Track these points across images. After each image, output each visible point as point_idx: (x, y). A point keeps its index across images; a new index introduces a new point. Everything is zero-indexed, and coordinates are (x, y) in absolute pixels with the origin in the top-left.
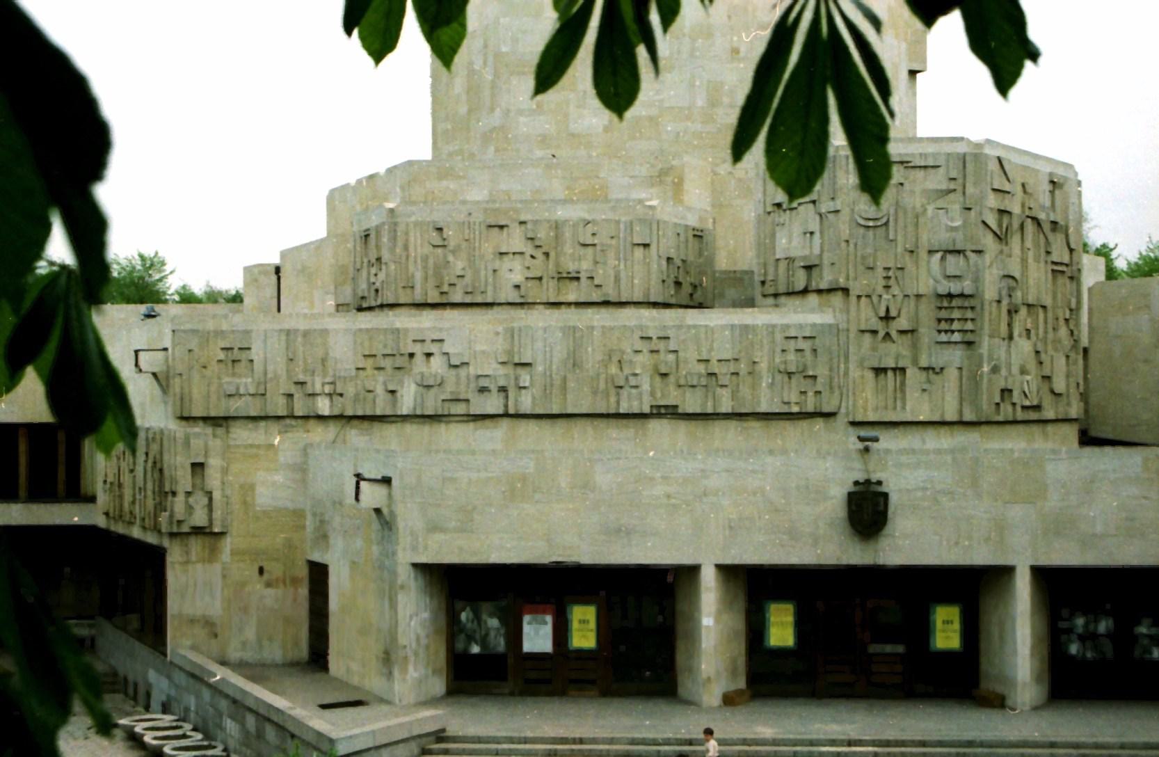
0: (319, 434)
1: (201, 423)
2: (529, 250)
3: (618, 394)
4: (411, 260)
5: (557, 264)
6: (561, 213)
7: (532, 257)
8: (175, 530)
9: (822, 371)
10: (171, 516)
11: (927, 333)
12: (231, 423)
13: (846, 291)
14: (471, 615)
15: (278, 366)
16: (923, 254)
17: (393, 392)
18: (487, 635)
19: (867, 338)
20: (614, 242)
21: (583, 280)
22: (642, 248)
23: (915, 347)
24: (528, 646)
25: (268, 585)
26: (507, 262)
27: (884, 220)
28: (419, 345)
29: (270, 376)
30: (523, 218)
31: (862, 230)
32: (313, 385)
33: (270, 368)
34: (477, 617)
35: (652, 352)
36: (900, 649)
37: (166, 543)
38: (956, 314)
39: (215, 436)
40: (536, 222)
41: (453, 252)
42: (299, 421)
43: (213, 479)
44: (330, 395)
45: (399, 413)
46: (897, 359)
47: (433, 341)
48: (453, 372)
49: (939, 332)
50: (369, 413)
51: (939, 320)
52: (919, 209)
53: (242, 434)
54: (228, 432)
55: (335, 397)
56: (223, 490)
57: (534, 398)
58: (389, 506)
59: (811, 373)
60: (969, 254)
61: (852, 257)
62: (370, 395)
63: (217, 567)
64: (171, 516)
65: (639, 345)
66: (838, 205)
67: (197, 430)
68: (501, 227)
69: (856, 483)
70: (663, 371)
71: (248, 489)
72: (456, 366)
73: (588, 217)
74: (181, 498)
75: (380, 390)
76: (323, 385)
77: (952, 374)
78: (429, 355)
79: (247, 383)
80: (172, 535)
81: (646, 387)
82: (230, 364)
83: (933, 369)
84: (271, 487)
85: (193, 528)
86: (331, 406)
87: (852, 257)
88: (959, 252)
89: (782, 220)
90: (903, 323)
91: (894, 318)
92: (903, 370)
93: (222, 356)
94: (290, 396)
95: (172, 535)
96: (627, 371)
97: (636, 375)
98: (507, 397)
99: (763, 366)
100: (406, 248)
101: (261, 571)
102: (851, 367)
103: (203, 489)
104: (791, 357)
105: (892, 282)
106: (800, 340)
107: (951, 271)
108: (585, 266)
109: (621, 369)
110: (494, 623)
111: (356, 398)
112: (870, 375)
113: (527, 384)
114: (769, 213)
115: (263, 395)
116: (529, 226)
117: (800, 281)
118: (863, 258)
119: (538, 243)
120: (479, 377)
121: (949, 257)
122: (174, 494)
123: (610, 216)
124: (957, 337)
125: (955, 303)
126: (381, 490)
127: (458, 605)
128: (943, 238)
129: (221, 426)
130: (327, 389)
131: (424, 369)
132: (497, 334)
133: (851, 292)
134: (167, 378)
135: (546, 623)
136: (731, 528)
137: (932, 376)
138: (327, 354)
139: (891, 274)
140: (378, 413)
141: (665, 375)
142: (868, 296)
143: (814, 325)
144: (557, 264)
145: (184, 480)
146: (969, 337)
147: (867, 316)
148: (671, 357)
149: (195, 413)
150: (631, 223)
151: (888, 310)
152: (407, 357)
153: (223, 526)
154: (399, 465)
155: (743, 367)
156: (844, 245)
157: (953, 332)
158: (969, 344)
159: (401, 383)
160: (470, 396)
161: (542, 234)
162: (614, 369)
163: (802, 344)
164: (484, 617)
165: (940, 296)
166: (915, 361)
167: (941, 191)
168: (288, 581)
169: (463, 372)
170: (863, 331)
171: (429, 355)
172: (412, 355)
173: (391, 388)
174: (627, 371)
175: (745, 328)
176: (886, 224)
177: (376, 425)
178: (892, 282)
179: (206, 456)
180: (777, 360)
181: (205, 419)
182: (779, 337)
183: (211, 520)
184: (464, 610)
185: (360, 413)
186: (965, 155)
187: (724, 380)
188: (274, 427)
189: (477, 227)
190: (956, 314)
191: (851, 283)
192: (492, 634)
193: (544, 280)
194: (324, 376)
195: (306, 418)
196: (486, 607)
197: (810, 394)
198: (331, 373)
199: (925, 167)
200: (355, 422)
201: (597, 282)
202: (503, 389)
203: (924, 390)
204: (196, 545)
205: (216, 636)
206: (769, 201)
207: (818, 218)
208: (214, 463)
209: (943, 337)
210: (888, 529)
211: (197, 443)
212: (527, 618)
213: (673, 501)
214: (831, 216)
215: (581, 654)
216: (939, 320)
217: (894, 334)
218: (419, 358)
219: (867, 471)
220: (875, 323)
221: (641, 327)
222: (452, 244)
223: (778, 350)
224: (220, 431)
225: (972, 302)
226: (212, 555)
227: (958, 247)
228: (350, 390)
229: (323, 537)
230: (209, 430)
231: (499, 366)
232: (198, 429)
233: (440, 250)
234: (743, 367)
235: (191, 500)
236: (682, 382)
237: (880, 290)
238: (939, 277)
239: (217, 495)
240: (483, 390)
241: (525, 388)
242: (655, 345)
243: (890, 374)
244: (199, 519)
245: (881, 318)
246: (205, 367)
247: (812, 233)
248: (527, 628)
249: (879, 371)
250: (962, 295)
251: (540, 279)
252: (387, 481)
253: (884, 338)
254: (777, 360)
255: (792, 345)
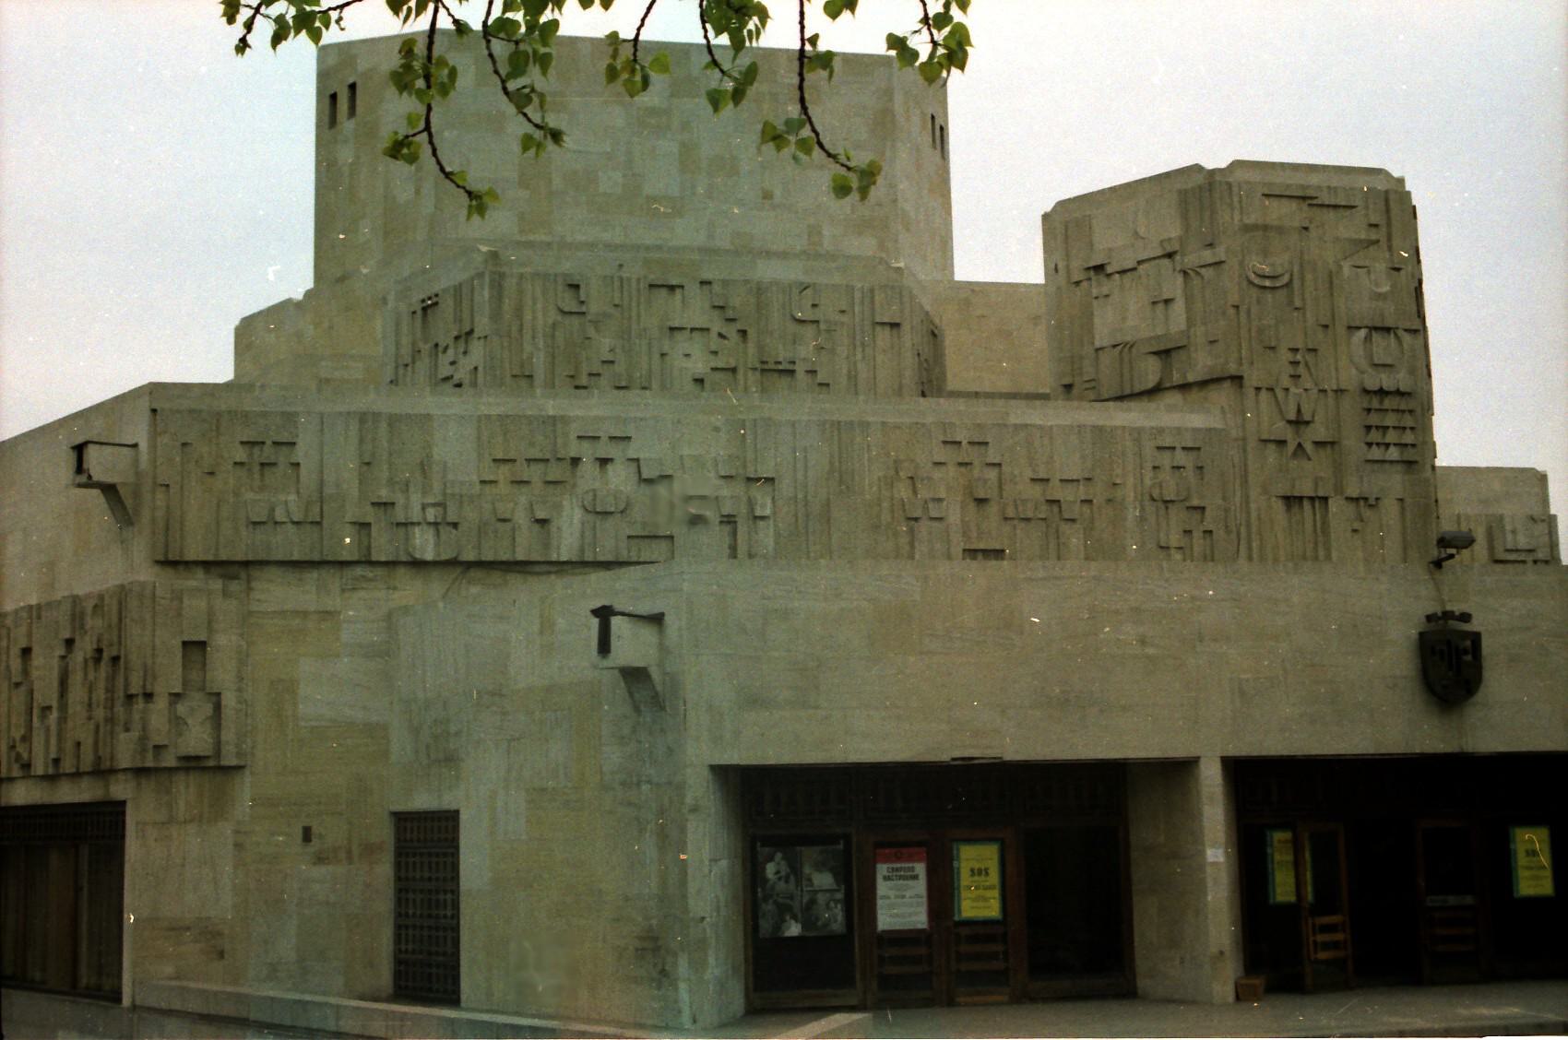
0: (409, 590)
1: (200, 573)
2: (717, 326)
3: (911, 531)
4: (527, 336)
5: (761, 348)
6: (768, 271)
7: (721, 335)
8: (150, 763)
9: (1213, 503)
10: (144, 738)
11: (1352, 441)
12: (255, 572)
13: (1237, 379)
14: (784, 869)
15: (343, 468)
16: (1341, 330)
17: (543, 522)
18: (813, 902)
19: (1271, 454)
20: (844, 319)
21: (800, 374)
22: (888, 328)
23: (1338, 468)
24: (887, 919)
25: (320, 859)
26: (683, 343)
27: (1286, 279)
28: (586, 444)
29: (328, 491)
30: (707, 276)
31: (1254, 292)
32: (406, 507)
33: (330, 477)
34: (795, 870)
35: (960, 464)
36: (1469, 900)
37: (120, 789)
38: (1390, 420)
39: (226, 594)
40: (725, 283)
41: (596, 323)
42: (379, 571)
43: (222, 672)
44: (436, 524)
45: (554, 557)
46: (1316, 481)
47: (612, 438)
48: (645, 489)
49: (1370, 445)
50: (505, 556)
51: (1368, 428)
52: (1333, 267)
53: (274, 593)
54: (250, 589)
55: (444, 530)
56: (240, 690)
57: (778, 535)
58: (661, 665)
59: (1195, 502)
60: (1400, 333)
61: (1244, 332)
62: (508, 526)
63: (227, 828)
64: (144, 738)
65: (941, 454)
66: (1220, 253)
67: (192, 583)
68: (672, 288)
69: (1429, 618)
70: (982, 495)
71: (284, 690)
72: (649, 481)
73: (807, 280)
74: (161, 703)
75: (521, 518)
76: (424, 507)
77: (1390, 510)
78: (604, 462)
79: (290, 503)
80: (140, 772)
81: (954, 517)
82: (257, 468)
83: (1366, 499)
84: (327, 686)
85: (187, 758)
86: (437, 544)
87: (1244, 332)
88: (1388, 330)
89: (1105, 290)
90: (1320, 431)
91: (1307, 423)
92: (1325, 499)
93: (240, 454)
94: (365, 526)
95: (140, 772)
96: (924, 493)
97: (940, 500)
98: (734, 533)
99: (1129, 493)
100: (519, 311)
101: (307, 835)
102: (1254, 493)
103: (203, 689)
104: (1166, 475)
105: (1301, 370)
106: (1179, 452)
107: (1380, 357)
108: (806, 351)
109: (915, 492)
110: (824, 880)
111: (482, 529)
112: (1279, 506)
113: (768, 512)
114: (1077, 283)
115: (318, 523)
116: (716, 288)
117: (1150, 372)
118: (1260, 331)
119: (730, 314)
120: (689, 499)
121: (1376, 336)
122: (149, 696)
123: (837, 279)
124: (1393, 453)
125: (1388, 403)
126: (648, 633)
127: (763, 851)
128: (1364, 308)
129: (236, 577)
130: (431, 514)
131: (597, 485)
132: (717, 429)
133: (1246, 382)
134: (137, 494)
135: (915, 877)
136: (1242, 693)
137: (1367, 513)
138: (429, 456)
139: (1299, 357)
140: (520, 556)
141: (981, 502)
142: (1271, 389)
143: (1195, 430)
144: (761, 348)
145: (171, 675)
146: (1410, 454)
147: (1264, 417)
148: (992, 474)
149: (191, 555)
150: (872, 291)
151: (1299, 411)
152: (567, 465)
153: (239, 755)
154: (686, 586)
155: (1099, 493)
156: (1232, 311)
157: (1387, 445)
158: (1410, 464)
159: (558, 507)
160: (675, 531)
161: (737, 300)
162: (903, 491)
163: (1181, 458)
164: (807, 870)
165: (1366, 391)
166: (1339, 489)
167: (1361, 241)
168: (356, 850)
169: (662, 490)
170: (1265, 441)
171: (604, 462)
172: (575, 461)
173: (541, 515)
174: (924, 493)
175: (1099, 430)
176: (1289, 285)
177: (515, 580)
178: (1301, 370)
179: (210, 630)
180: (1148, 482)
181: (206, 565)
182: (1149, 450)
183: (218, 744)
184: (771, 859)
185: (488, 556)
186: (1387, 192)
187: (1076, 511)
188: (333, 580)
189: (634, 284)
190: (1390, 420)
191: (1245, 367)
192: (821, 898)
193: (740, 375)
194: (424, 493)
195: (391, 564)
196: (810, 854)
197: (1197, 534)
198: (437, 486)
199: (1336, 207)
200: (475, 574)
201: (820, 378)
202: (729, 520)
203: (1355, 531)
204: (186, 791)
205: (221, 955)
206: (1077, 264)
207: (1180, 279)
208: (224, 642)
209: (1376, 453)
210: (1479, 697)
211: (195, 606)
212: (882, 869)
213: (1151, 651)
214: (1208, 273)
215: (980, 928)
216: (1368, 428)
217: (1309, 447)
218: (588, 467)
219: (1443, 602)
220: (1280, 429)
221: (945, 426)
222: (594, 308)
223: (1149, 465)
224: (235, 586)
225: (1412, 404)
226: (218, 807)
227: (1389, 323)
228: (470, 515)
229: (443, 757)
230: (217, 584)
231: (722, 482)
232: (197, 580)
233: (576, 321)
234: (1099, 493)
235: (181, 709)
236: (1010, 512)
237: (1286, 382)
238: (1364, 364)
239: (229, 700)
240: (696, 520)
241: (763, 518)
242: (968, 453)
243: (1306, 504)
244: (196, 739)
245: (1290, 422)
246: (211, 473)
247: (1167, 302)
248: (883, 888)
249: (1291, 501)
250: (1399, 393)
251: (734, 370)
252: (657, 620)
253: (1295, 454)
254: (1148, 482)
255: (1166, 460)
